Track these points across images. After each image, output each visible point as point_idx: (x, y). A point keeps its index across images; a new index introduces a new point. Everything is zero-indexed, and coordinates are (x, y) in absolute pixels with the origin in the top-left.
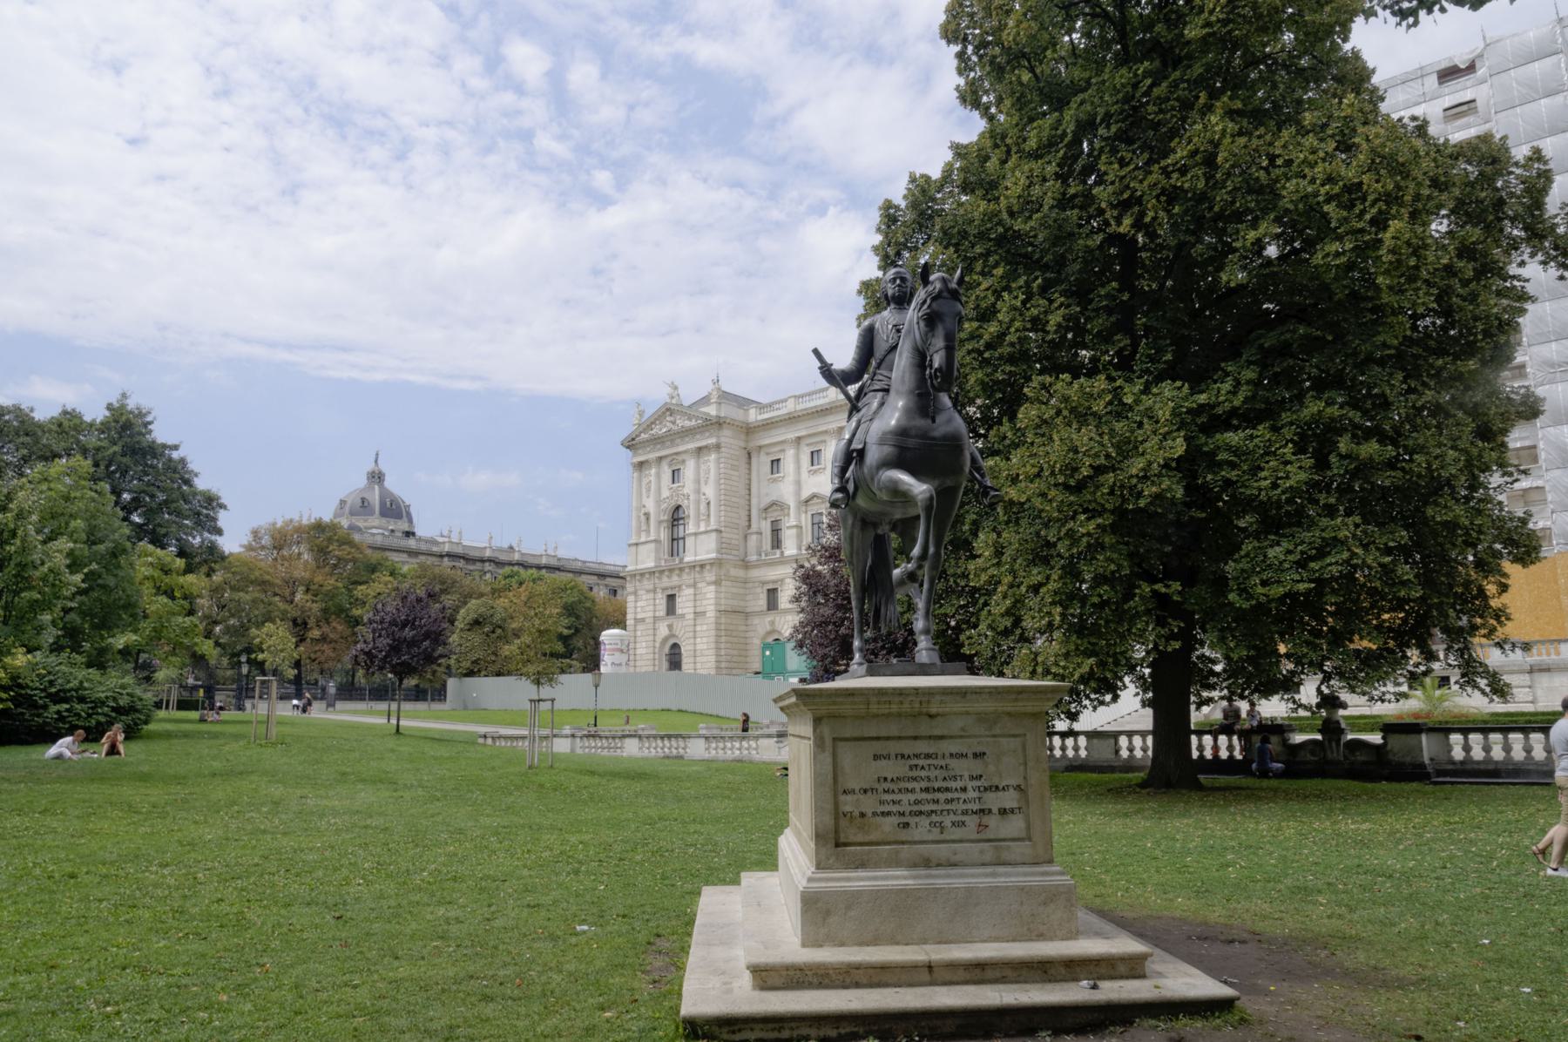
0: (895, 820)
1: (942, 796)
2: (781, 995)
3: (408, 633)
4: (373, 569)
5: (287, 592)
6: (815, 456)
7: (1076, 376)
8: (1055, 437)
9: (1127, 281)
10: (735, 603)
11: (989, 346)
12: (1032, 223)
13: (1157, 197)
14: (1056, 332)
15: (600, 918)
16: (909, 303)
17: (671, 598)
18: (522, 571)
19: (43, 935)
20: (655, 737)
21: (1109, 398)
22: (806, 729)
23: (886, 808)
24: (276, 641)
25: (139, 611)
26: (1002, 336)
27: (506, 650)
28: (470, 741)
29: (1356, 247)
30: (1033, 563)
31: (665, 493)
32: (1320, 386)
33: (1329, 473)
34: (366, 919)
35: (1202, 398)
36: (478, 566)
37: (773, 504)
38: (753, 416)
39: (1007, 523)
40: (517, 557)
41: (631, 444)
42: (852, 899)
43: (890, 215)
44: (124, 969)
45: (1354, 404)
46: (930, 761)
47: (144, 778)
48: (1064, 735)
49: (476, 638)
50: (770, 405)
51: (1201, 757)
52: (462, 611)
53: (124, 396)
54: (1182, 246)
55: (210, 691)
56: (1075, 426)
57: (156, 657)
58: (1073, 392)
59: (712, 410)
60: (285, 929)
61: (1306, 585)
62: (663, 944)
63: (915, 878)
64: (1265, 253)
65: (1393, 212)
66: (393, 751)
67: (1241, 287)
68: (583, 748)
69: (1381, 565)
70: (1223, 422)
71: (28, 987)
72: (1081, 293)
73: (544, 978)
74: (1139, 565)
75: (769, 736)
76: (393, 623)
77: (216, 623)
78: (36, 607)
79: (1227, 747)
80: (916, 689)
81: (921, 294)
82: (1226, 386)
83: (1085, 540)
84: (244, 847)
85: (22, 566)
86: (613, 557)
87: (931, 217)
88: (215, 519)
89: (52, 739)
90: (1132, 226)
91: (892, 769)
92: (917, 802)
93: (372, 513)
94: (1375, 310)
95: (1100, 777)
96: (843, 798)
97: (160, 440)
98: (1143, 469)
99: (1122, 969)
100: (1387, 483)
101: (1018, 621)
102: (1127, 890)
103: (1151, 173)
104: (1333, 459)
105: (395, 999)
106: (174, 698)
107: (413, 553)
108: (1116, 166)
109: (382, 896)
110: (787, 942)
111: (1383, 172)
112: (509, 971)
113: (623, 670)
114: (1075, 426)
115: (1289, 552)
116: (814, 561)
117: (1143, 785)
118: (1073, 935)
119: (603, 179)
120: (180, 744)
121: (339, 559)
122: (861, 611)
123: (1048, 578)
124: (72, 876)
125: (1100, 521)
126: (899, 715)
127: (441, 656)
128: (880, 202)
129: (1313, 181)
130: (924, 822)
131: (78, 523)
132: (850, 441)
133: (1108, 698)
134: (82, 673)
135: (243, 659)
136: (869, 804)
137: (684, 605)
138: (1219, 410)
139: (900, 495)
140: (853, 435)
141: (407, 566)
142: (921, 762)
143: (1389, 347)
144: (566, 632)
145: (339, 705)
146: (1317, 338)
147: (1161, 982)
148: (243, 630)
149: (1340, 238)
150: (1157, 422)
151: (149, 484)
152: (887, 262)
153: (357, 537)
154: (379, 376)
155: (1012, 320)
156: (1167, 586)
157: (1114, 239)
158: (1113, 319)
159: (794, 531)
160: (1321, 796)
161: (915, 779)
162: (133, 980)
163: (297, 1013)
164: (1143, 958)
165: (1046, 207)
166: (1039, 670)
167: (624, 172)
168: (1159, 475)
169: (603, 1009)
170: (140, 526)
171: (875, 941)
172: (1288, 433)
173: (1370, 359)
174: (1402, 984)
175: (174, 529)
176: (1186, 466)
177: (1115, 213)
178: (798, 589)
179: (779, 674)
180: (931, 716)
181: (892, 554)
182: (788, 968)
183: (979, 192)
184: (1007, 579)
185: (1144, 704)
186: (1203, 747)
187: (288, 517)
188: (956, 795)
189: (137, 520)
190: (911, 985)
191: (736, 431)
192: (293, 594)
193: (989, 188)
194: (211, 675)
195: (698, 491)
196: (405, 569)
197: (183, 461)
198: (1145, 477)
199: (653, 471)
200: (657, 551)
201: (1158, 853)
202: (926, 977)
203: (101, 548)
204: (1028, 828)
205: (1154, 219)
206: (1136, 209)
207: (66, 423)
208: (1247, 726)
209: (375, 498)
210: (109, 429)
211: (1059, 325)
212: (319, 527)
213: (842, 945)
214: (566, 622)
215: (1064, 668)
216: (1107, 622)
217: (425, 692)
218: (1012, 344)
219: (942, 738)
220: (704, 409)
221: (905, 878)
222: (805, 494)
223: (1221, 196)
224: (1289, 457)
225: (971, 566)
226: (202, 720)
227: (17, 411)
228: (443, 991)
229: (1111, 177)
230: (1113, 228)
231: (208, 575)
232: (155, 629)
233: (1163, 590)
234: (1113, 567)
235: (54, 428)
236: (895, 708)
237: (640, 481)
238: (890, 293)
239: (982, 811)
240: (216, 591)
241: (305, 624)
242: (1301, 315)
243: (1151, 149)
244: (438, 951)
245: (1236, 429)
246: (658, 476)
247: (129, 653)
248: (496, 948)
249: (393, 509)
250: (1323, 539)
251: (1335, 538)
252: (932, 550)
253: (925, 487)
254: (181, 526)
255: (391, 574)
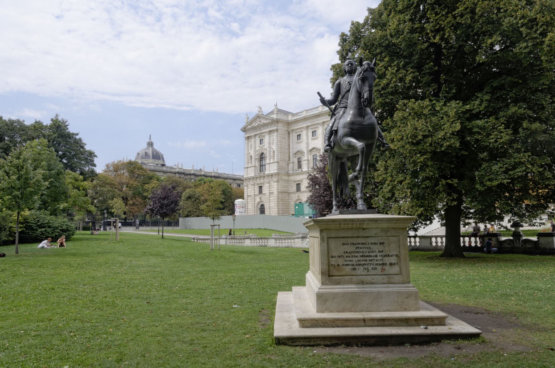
0: (350, 267)
1: (368, 259)
2: (309, 329)
3: (165, 202)
4: (151, 178)
5: (120, 188)
6: (314, 133)
7: (417, 100)
8: (409, 124)
9: (437, 62)
10: (284, 189)
11: (383, 89)
12: (399, 40)
13: (450, 27)
14: (409, 83)
15: (241, 303)
16: (355, 73)
17: (261, 187)
18: (205, 178)
19: (46, 309)
20: (256, 239)
21: (430, 108)
22: (317, 234)
23: (347, 263)
24: (118, 205)
25: (68, 195)
26: (388, 84)
27: (203, 207)
28: (189, 240)
29: (533, 45)
30: (398, 172)
31: (258, 148)
32: (516, 101)
33: (519, 136)
34: (158, 303)
35: (468, 107)
36: (189, 176)
37: (298, 151)
38: (290, 118)
39: (390, 157)
40: (203, 173)
41: (244, 130)
42: (335, 296)
43: (344, 39)
44: (75, 320)
45: (530, 108)
46: (364, 246)
47: (74, 255)
48: (415, 237)
49: (189, 203)
50: (297, 114)
51: (464, 245)
52: (184, 193)
53: (57, 115)
54: (461, 46)
55: (94, 224)
56: (416, 119)
57: (74, 211)
58: (416, 106)
59: (274, 116)
60: (130, 307)
61: (507, 180)
62: (265, 312)
63: (358, 288)
64: (495, 48)
65: (549, 29)
66: (161, 244)
67: (483, 63)
68: (231, 243)
69: (538, 172)
70: (477, 116)
71: (43, 327)
72: (419, 67)
73: (223, 323)
74: (442, 172)
75: (298, 238)
76: (160, 198)
77: (95, 199)
78: (32, 194)
79: (474, 242)
80: (358, 219)
81: (359, 69)
82: (477, 102)
83: (419, 164)
84: (112, 278)
85: (27, 179)
86: (239, 172)
87: (360, 38)
88: (93, 161)
89: (40, 241)
90: (440, 39)
91: (351, 248)
92: (359, 261)
93: (149, 158)
94: (539, 70)
95: (425, 252)
96: (331, 259)
97: (71, 132)
98: (443, 136)
99: (436, 322)
100: (542, 139)
101: (393, 194)
102: (436, 294)
103: (448, 17)
104: (520, 130)
105: (171, 330)
106: (81, 226)
107: (165, 172)
108: (434, 15)
109: (163, 296)
110: (311, 310)
111: (546, 13)
112: (211, 321)
113: (243, 214)
114: (416, 119)
115: (501, 167)
116: (315, 173)
117: (442, 256)
118: (418, 309)
119: (235, 26)
120: (85, 243)
121: (138, 175)
122: (336, 191)
123: (405, 178)
124: (53, 289)
125: (425, 157)
126: (352, 229)
127: (177, 210)
128: (340, 34)
129: (516, 18)
130: (361, 268)
131: (44, 163)
132: (332, 127)
133: (428, 222)
134: (49, 218)
135: (105, 212)
136: (341, 261)
137: (265, 190)
138: (474, 112)
139: (351, 147)
140: (333, 125)
141: (163, 177)
142: (360, 246)
143: (546, 85)
144: (223, 200)
145: (141, 228)
146: (515, 82)
147: (451, 327)
148: (105, 201)
149: (526, 41)
150: (449, 117)
151: (68, 148)
152: (343, 58)
153: (144, 167)
154: (152, 106)
155: (392, 78)
156: (452, 181)
157: (433, 45)
158: (431, 78)
159: (306, 162)
160: (512, 261)
161: (358, 252)
162: (78, 324)
163: (138, 335)
164: (445, 318)
165: (405, 33)
166: (402, 212)
167: (244, 23)
168: (450, 138)
169: (245, 334)
170: (66, 164)
171: (343, 311)
172: (502, 120)
173: (537, 90)
174: (545, 330)
175: (78, 165)
176: (460, 134)
177: (433, 34)
178: (309, 183)
179: (301, 215)
180: (364, 229)
181: (347, 168)
182: (312, 320)
183: (379, 28)
184: (390, 179)
185: (442, 225)
186: (465, 242)
187: (119, 160)
188: (373, 258)
189: (65, 161)
190: (357, 327)
191: (282, 123)
192: (122, 188)
193: (383, 26)
194: (94, 218)
195: (270, 147)
196: (162, 178)
197: (80, 139)
198: (444, 139)
199: (253, 140)
200: (255, 170)
201: (448, 281)
202: (363, 324)
203: (53, 172)
204: (400, 270)
205: (449, 36)
206: (442, 32)
207: (37, 126)
208: (482, 234)
209: (150, 152)
210: (53, 128)
211: (410, 81)
212: (130, 163)
213: (332, 312)
214: (223, 196)
215: (411, 212)
216: (429, 194)
217: (171, 223)
218: (392, 88)
219: (368, 237)
220: (272, 116)
221: (355, 288)
222: (310, 148)
223: (477, 26)
224: (503, 130)
225: (376, 174)
226: (92, 234)
227: (18, 121)
228: (188, 328)
229: (431, 20)
230: (432, 40)
231: (92, 181)
232: (74, 202)
233: (451, 182)
234: (432, 174)
235: (33, 128)
236: (350, 226)
237: (248, 143)
238: (347, 69)
239: (383, 264)
240: (95, 187)
241: (127, 199)
242: (509, 73)
243: (449, 8)
244: (184, 314)
245: (480, 119)
246: (255, 142)
247: (65, 210)
248: (205, 313)
249: (157, 156)
250: (515, 162)
251: (520, 162)
252: (363, 167)
253: (361, 144)
254: (81, 164)
255: (157, 180)
